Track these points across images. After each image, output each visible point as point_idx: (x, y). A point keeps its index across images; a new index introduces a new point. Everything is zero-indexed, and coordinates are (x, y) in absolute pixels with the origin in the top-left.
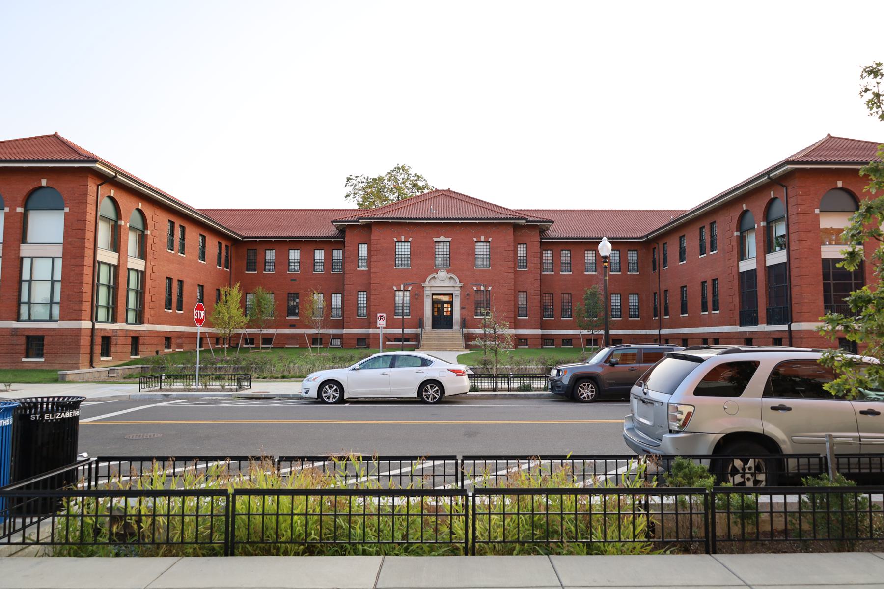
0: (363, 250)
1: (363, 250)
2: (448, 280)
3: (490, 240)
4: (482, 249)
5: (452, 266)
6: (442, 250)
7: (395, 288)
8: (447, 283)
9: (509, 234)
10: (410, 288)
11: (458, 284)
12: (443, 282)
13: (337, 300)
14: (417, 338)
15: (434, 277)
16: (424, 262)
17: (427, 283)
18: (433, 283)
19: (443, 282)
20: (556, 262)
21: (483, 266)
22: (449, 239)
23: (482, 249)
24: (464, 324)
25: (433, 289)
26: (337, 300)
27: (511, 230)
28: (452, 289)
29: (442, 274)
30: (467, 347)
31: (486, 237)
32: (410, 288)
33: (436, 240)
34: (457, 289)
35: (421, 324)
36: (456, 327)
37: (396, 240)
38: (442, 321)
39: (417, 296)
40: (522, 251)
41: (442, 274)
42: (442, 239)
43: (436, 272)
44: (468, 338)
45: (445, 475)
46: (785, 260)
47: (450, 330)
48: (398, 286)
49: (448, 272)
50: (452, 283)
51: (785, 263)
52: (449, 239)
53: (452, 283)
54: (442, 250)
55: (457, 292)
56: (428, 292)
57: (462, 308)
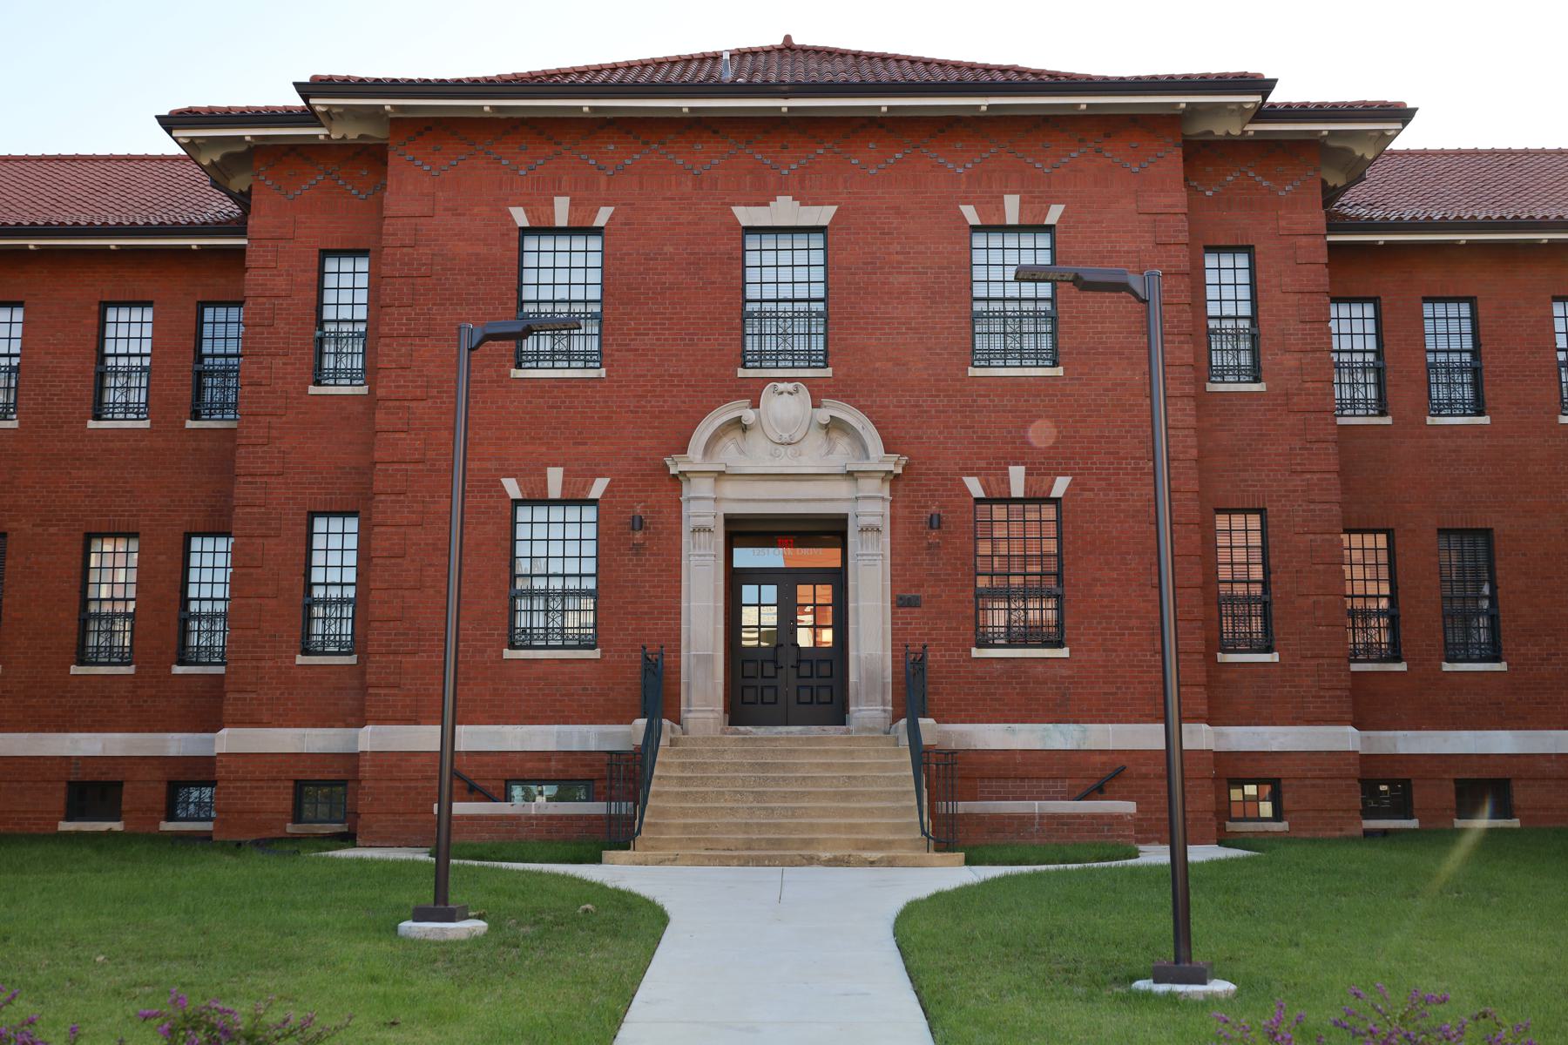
0: (347, 290)
1: (347, 290)
2: (817, 438)
3: (1054, 215)
4: (1001, 267)
5: (843, 377)
6: (786, 274)
7: (512, 488)
8: (812, 458)
9: (1162, 183)
10: (598, 488)
11: (879, 459)
12: (785, 446)
13: (211, 569)
14: (625, 776)
15: (738, 424)
16: (685, 344)
17: (694, 458)
18: (729, 455)
19: (785, 446)
20: (1395, 362)
21: (1013, 361)
22: (822, 215)
23: (1001, 267)
24: (915, 690)
25: (730, 489)
26: (211, 569)
27: (1171, 162)
28: (843, 489)
29: (785, 407)
30: (947, 836)
31: (1035, 199)
32: (598, 488)
33: (746, 215)
34: (872, 487)
35: (656, 692)
36: (868, 710)
37: (520, 218)
38: (783, 686)
39: (638, 544)
40: (1227, 286)
41: (785, 407)
42: (784, 211)
43: (752, 392)
44: (943, 775)
45: (759, 605)
46: (460, 729)
47: (832, 731)
48: (533, 475)
49: (818, 392)
50: (841, 455)
51: (461, 724)
52: (822, 215)
53: (841, 455)
54: (786, 274)
55: (869, 509)
56: (703, 508)
57: (902, 602)
